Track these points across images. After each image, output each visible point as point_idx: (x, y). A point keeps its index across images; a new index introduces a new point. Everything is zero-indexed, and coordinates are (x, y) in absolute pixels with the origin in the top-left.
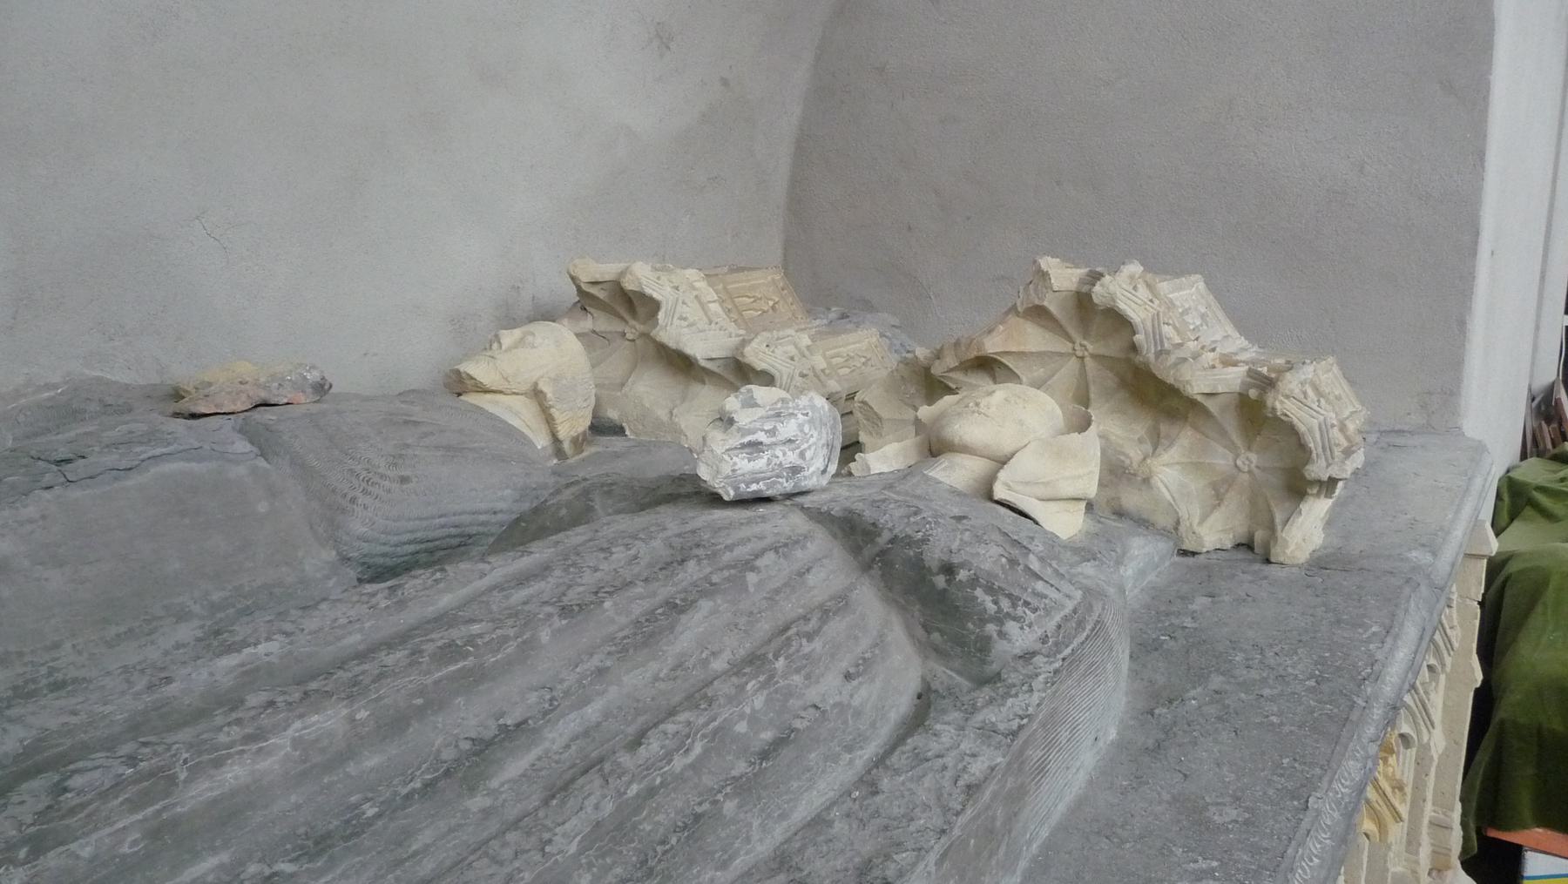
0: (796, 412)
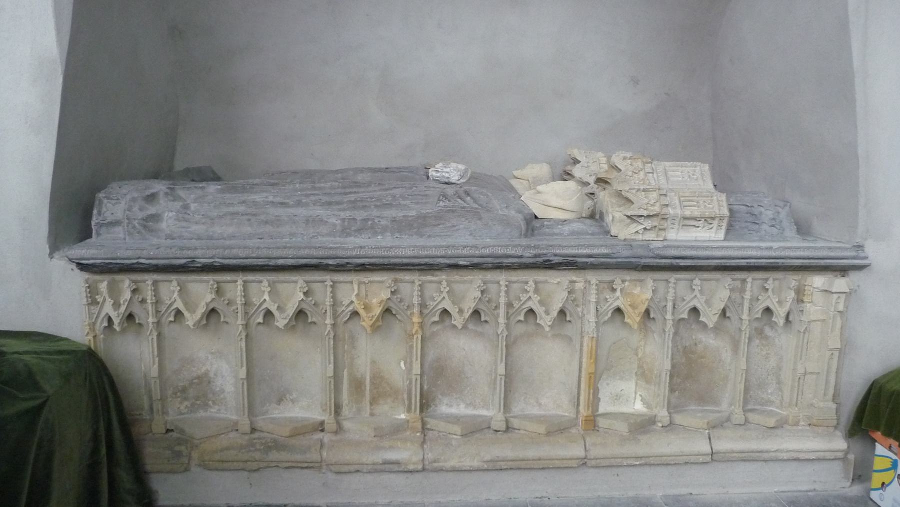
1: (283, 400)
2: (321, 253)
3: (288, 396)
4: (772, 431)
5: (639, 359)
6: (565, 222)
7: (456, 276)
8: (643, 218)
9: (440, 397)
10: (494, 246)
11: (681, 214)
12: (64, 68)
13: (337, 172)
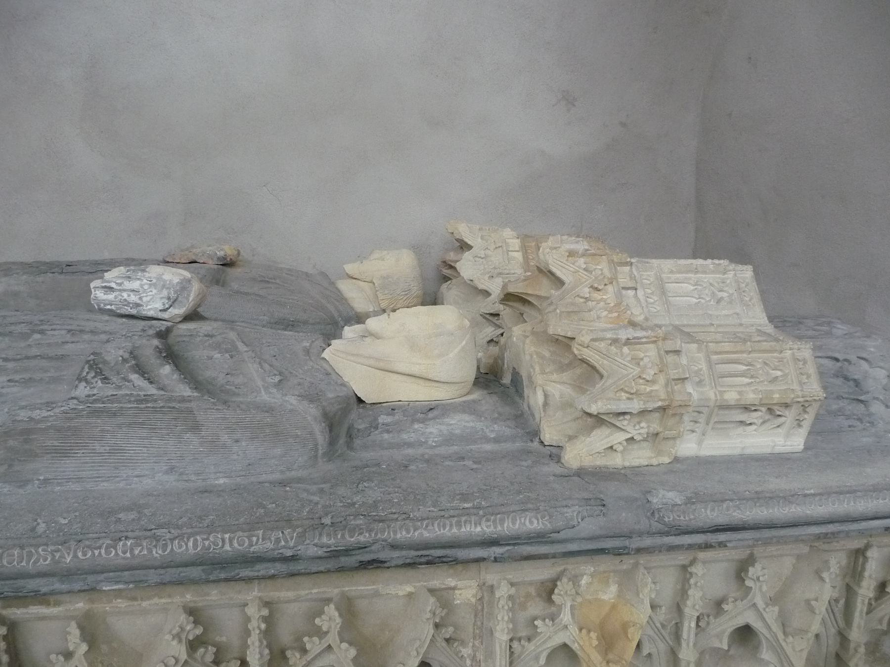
0: (142, 278)
6: (431, 415)
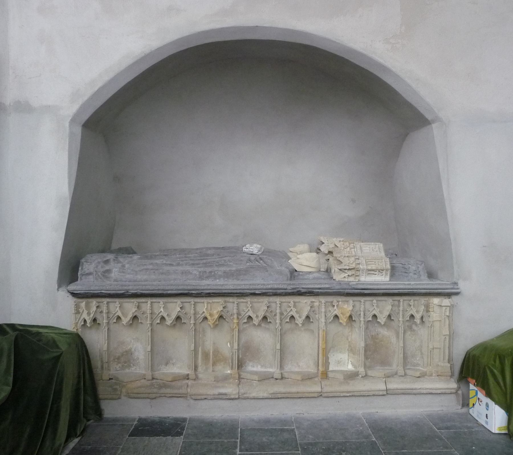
1: (168, 363)
2: (189, 288)
3: (171, 361)
4: (418, 378)
5: (349, 342)
7: (255, 299)
8: (347, 270)
9: (248, 362)
10: (273, 284)
11: (366, 268)
12: (71, 201)
13: (197, 249)
